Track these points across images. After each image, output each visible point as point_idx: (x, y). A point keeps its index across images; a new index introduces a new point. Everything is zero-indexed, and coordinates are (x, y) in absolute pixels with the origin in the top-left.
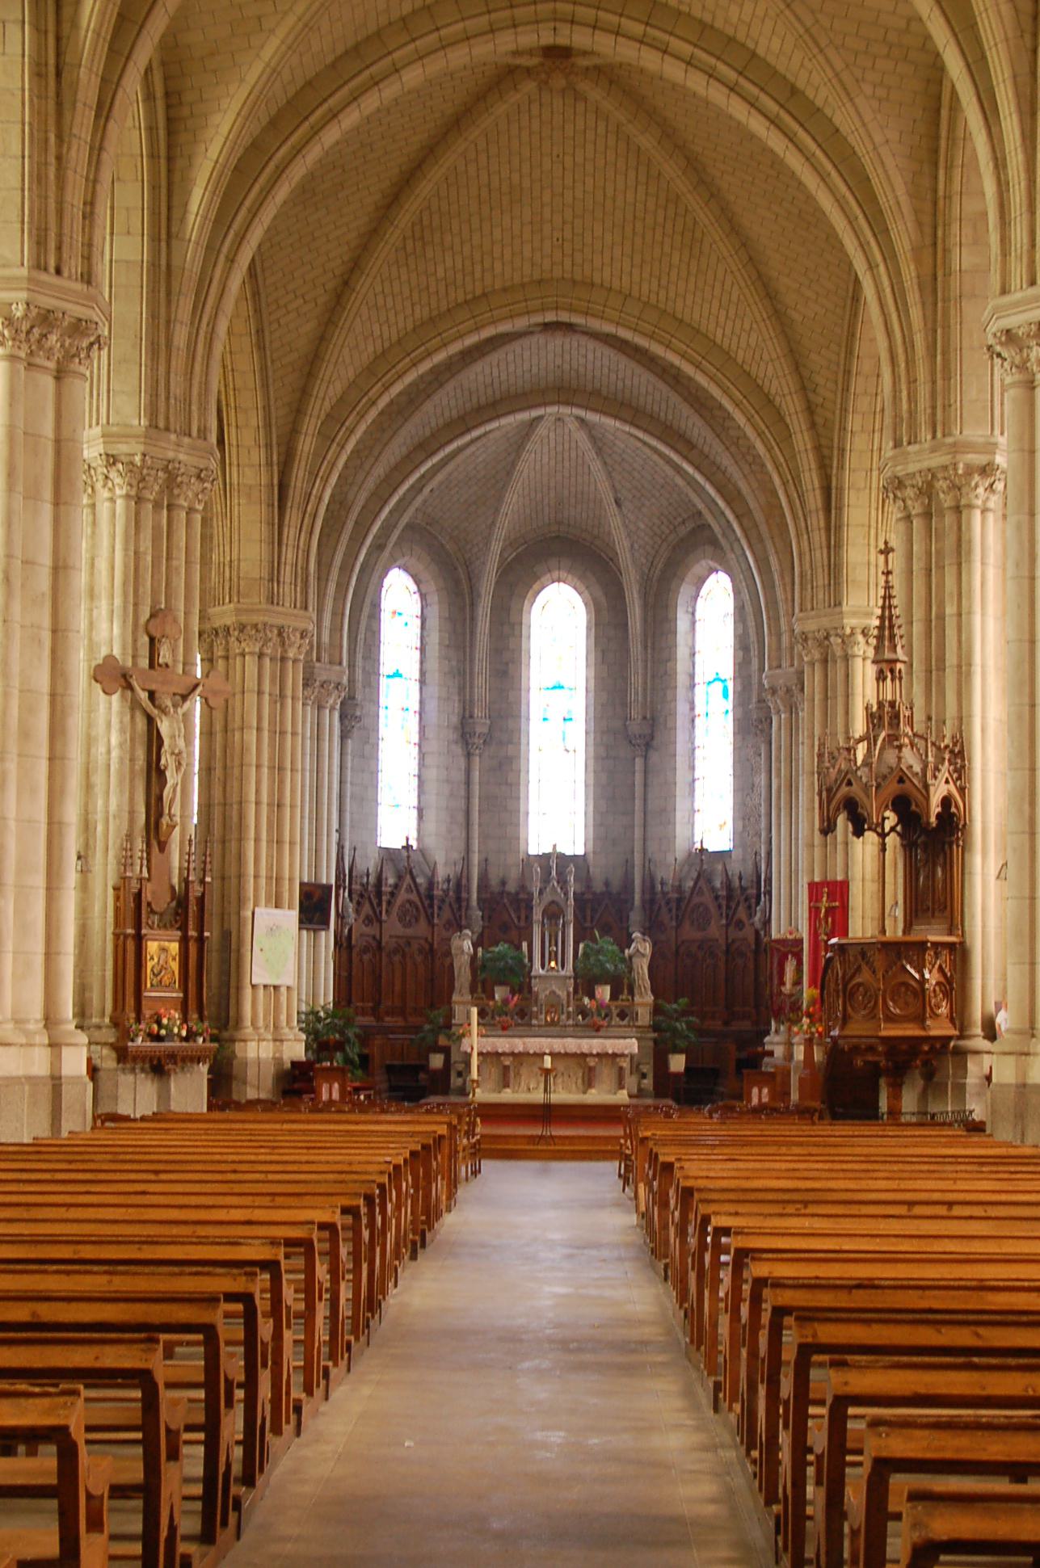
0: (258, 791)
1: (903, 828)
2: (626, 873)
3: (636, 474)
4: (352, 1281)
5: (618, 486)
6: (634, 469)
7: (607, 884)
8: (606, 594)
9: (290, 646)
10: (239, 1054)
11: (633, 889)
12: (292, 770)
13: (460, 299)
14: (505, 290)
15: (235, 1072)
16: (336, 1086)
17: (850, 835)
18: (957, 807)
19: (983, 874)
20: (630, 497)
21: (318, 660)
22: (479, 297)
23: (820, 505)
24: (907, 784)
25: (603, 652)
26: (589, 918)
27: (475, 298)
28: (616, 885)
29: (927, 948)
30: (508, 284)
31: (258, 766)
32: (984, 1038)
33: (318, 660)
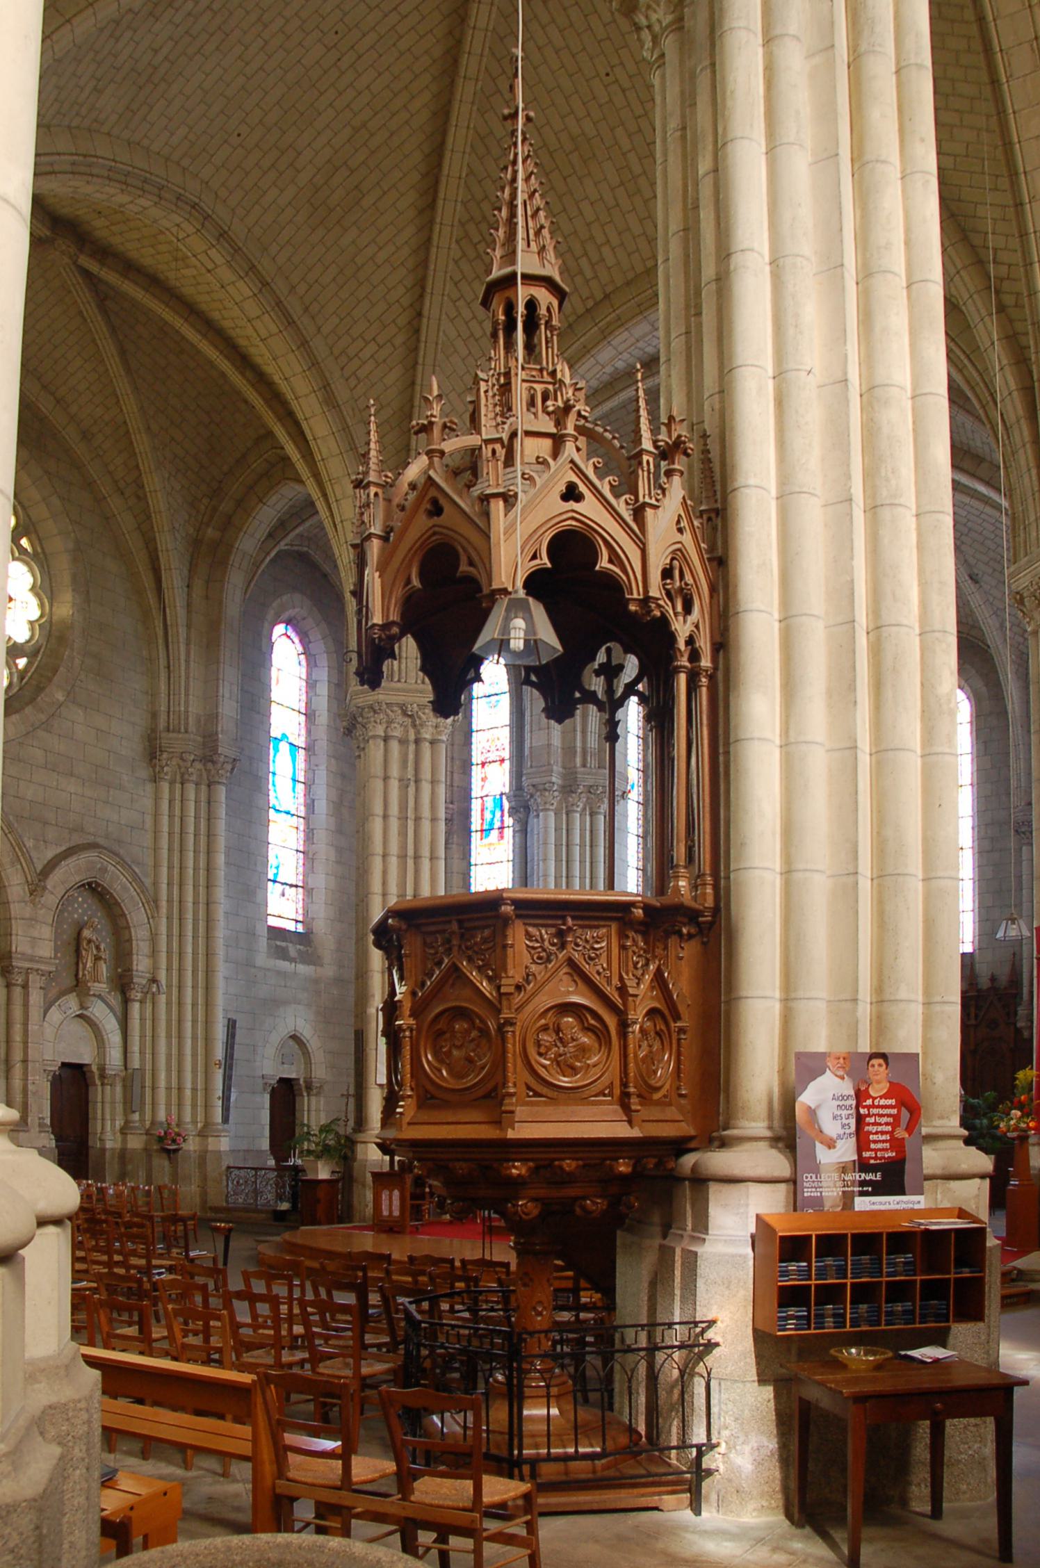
0: (384, 883)
1: (650, 684)
2: (1013, 964)
3: (988, 543)
4: (442, 1414)
5: (972, 561)
6: (987, 538)
7: (993, 979)
8: (986, 685)
9: (421, 725)
10: (360, 1156)
11: (1022, 984)
12: (431, 859)
13: (581, 310)
14: (628, 283)
15: (355, 1174)
16: (396, 1193)
17: (354, 680)
18: (614, 558)
19: (787, 746)
20: (990, 571)
21: (584, 765)
22: (601, 301)
23: (1021, 412)
24: (446, 518)
25: (985, 742)
26: (973, 1015)
27: (596, 304)
28: (1003, 979)
29: (506, 921)
30: (630, 275)
31: (385, 856)
32: (968, 1142)
33: (584, 765)
